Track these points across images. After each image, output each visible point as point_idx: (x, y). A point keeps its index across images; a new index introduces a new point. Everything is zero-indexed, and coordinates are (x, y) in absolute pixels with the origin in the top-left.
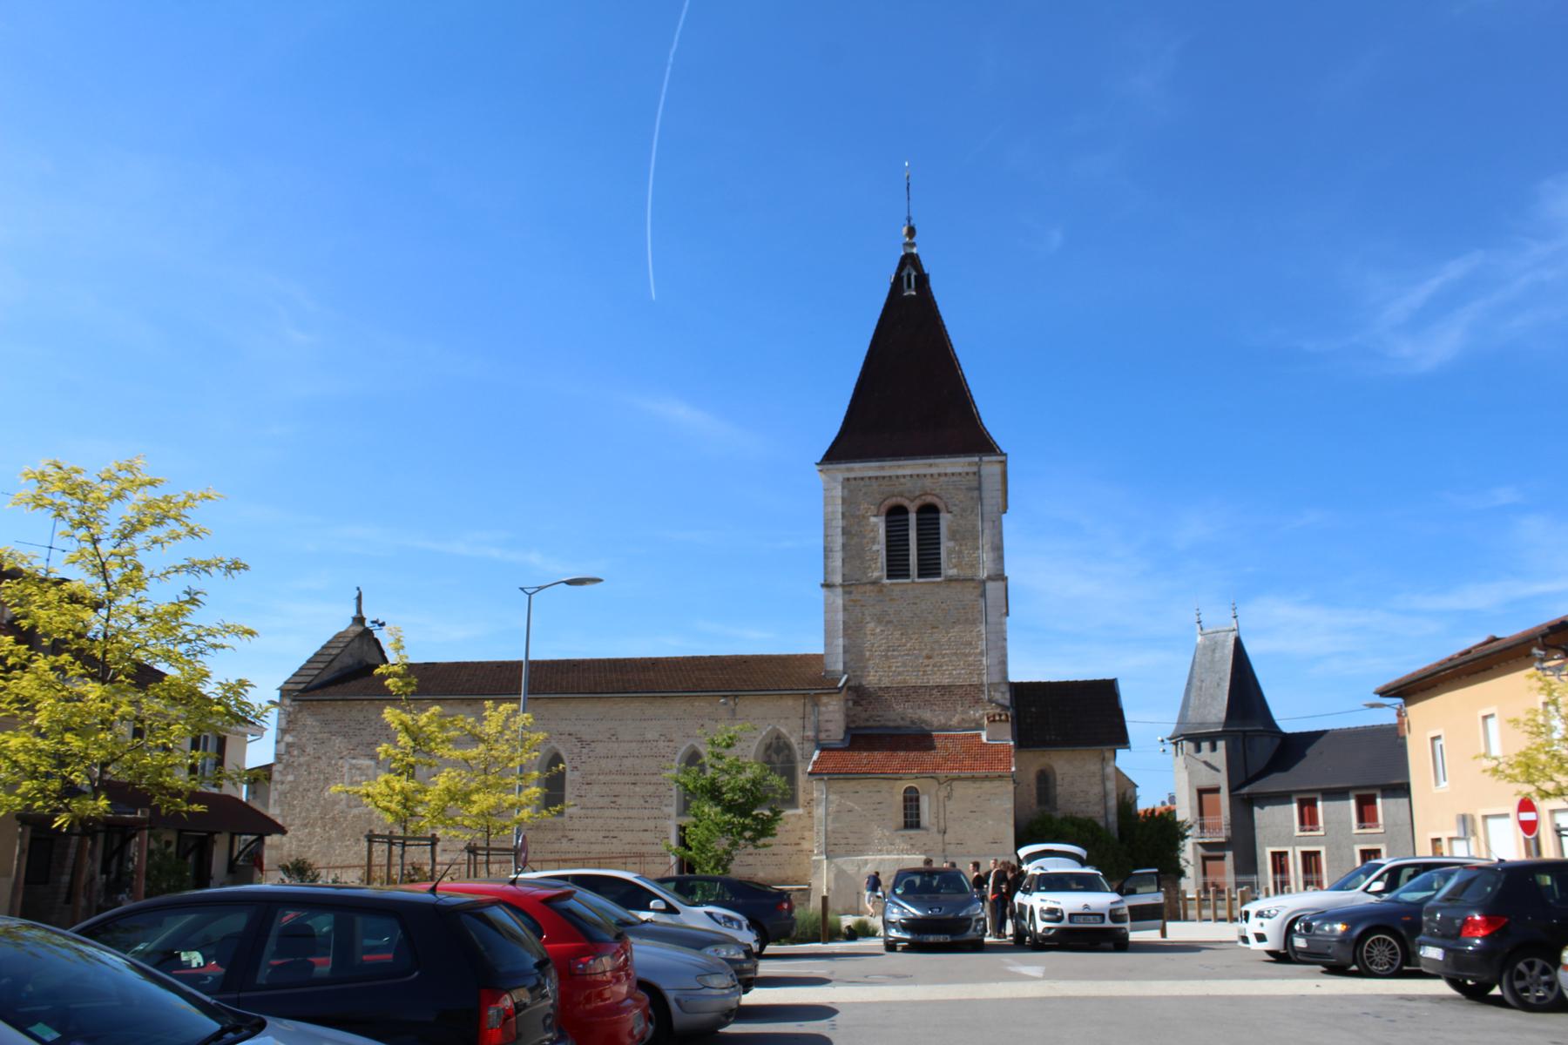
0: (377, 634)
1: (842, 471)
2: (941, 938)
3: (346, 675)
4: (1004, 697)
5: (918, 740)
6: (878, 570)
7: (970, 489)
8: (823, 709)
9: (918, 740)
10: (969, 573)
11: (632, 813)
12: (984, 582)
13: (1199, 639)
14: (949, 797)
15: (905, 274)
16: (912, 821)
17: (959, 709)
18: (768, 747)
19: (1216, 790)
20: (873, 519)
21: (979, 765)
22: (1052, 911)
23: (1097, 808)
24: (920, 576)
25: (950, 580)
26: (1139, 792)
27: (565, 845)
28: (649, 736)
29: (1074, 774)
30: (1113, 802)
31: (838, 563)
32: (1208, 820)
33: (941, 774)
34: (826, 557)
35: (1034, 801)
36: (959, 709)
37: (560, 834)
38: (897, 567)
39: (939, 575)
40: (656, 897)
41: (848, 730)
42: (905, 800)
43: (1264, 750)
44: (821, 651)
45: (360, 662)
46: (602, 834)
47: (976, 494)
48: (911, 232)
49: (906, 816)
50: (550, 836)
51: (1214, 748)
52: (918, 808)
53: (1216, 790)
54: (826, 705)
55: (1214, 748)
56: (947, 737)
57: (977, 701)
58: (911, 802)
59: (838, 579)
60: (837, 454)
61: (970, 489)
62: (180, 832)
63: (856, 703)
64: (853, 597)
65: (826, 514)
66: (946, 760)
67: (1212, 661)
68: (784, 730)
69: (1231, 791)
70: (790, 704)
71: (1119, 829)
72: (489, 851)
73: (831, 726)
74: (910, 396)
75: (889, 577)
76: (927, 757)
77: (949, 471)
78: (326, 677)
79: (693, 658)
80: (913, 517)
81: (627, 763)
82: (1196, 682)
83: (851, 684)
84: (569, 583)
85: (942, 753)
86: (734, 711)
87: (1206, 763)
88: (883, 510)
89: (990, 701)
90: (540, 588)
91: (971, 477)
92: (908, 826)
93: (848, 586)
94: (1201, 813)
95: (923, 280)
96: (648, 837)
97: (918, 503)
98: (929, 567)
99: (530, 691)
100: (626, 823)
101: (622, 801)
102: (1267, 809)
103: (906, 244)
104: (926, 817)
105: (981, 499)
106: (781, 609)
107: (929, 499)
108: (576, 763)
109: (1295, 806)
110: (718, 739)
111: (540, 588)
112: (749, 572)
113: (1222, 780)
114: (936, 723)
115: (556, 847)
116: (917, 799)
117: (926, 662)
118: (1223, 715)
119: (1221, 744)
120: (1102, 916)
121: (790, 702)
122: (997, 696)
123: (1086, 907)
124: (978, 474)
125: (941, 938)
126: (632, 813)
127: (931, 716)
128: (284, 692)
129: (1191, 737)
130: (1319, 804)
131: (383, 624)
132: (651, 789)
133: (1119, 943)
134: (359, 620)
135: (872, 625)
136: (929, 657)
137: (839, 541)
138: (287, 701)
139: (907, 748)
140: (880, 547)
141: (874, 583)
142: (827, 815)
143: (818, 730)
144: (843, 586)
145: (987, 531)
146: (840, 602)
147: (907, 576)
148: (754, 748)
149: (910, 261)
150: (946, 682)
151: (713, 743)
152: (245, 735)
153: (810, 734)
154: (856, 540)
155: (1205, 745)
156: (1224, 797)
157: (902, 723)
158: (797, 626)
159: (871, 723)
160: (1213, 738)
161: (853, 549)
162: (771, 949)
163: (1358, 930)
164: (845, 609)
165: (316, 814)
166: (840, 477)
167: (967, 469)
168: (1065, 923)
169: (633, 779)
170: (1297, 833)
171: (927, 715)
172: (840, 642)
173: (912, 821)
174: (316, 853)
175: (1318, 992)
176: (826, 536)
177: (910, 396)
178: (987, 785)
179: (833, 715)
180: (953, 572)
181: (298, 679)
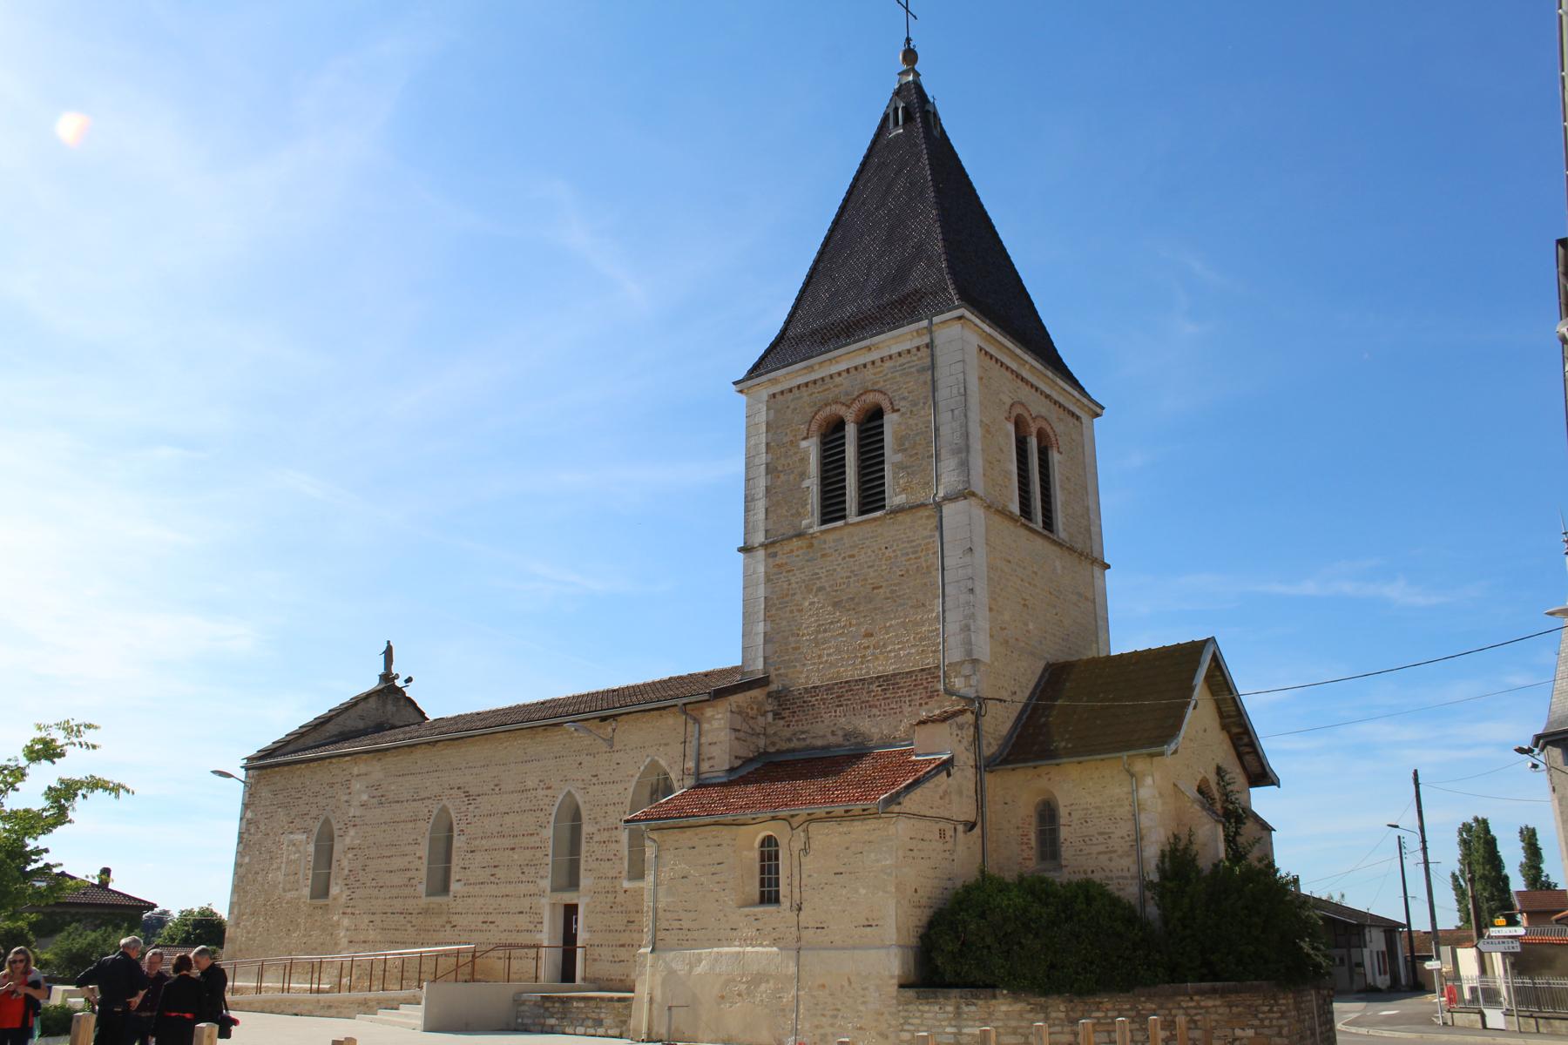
6: (811, 519)
7: (922, 370)
10: (920, 497)
11: (509, 889)
14: (805, 850)
17: (907, 709)
24: (861, 512)
25: (900, 510)
28: (530, 784)
31: (762, 516)
34: (747, 510)
36: (907, 709)
37: (445, 919)
38: (832, 509)
44: (1252, 790)
46: (481, 918)
48: (910, 56)
49: (762, 884)
54: (709, 721)
57: (932, 694)
58: (769, 853)
59: (760, 538)
61: (922, 370)
63: (777, 715)
64: (778, 560)
65: (748, 449)
73: (715, 751)
77: (894, 350)
80: (851, 431)
81: (508, 820)
88: (814, 427)
96: (522, 921)
97: (856, 406)
98: (872, 499)
100: (504, 902)
101: (500, 873)
102: (1277, 865)
107: (871, 398)
108: (463, 826)
117: (865, 642)
124: (930, 346)
126: (509, 889)
127: (872, 726)
130: (1222, 855)
131: (409, 680)
132: (528, 853)
134: (387, 677)
136: (869, 635)
137: (762, 483)
140: (812, 483)
146: (761, 569)
149: (913, 110)
150: (890, 669)
153: (691, 764)
154: (783, 477)
157: (832, 740)
159: (794, 744)
164: (768, 580)
165: (261, 901)
166: (764, 394)
169: (508, 842)
176: (747, 480)
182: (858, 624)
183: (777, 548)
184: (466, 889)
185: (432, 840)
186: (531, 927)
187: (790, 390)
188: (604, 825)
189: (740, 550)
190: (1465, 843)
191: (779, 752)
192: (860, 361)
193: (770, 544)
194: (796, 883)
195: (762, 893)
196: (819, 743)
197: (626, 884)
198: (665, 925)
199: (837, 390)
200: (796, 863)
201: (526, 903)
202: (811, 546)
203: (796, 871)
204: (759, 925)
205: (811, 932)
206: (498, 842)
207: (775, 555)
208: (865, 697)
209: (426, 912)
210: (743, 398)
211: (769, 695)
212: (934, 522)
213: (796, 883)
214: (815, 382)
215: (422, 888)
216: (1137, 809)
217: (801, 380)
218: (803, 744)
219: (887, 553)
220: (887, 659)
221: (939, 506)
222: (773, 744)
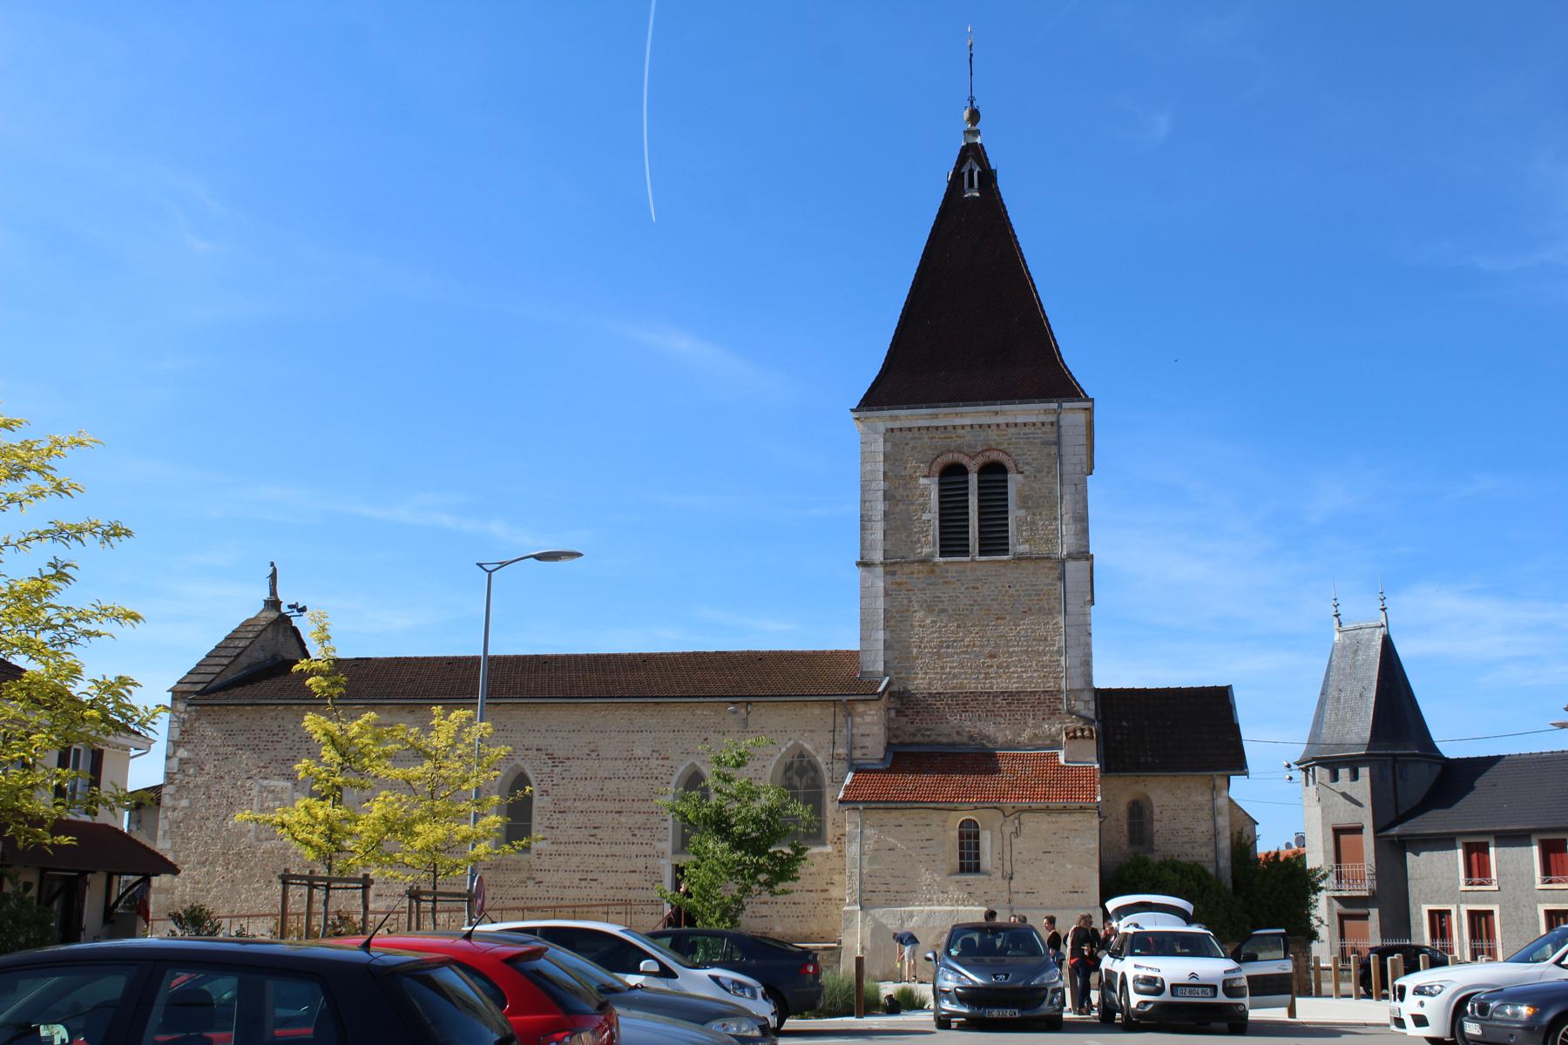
0: (296, 622)
1: (884, 419)
2: (1008, 1013)
3: (256, 674)
4: (1088, 708)
5: (977, 760)
6: (929, 545)
7: (1046, 443)
8: (858, 720)
9: (977, 760)
10: (1043, 549)
11: (617, 849)
12: (1063, 562)
13: (1337, 636)
14: (1017, 833)
15: (965, 170)
16: (969, 863)
17: (1031, 722)
18: (788, 768)
19: (1358, 830)
20: (922, 481)
21: (1055, 793)
22: (1149, 981)
23: (1204, 850)
24: (981, 553)
25: (1020, 558)
27: (531, 889)
28: (638, 752)
30: (1225, 843)
31: (879, 535)
33: (1008, 804)
34: (863, 528)
36: (1031, 722)
37: (524, 875)
38: (952, 542)
39: (1006, 552)
40: (648, 956)
41: (889, 746)
42: (961, 836)
43: (1420, 780)
44: (854, 645)
45: (274, 657)
46: (579, 875)
47: (1054, 449)
48: (975, 116)
49: (961, 856)
50: (514, 878)
51: (1355, 777)
52: (977, 846)
54: (861, 715)
55: (1355, 777)
57: (1054, 712)
58: (969, 839)
59: (878, 556)
60: (874, 400)
61: (1046, 443)
62: (43, 871)
63: (899, 713)
65: (863, 474)
66: (1013, 786)
67: (1353, 666)
68: (808, 746)
69: (1376, 831)
70: (816, 714)
72: (435, 896)
73: (868, 742)
74: (971, 323)
75: (942, 554)
76: (989, 781)
77: (1020, 420)
78: (230, 675)
80: (973, 479)
81: (611, 786)
82: (1332, 692)
83: (894, 688)
84: (539, 557)
86: (745, 721)
87: (1344, 795)
88: (936, 468)
89: (1070, 712)
90: (503, 564)
91: (1048, 428)
93: (890, 565)
95: (988, 178)
97: (980, 460)
98: (994, 542)
100: (609, 862)
102: (1424, 855)
103: (967, 132)
104: (987, 860)
107: (994, 456)
108: (547, 786)
109: (1460, 852)
111: (503, 564)
113: (1365, 817)
114: (1000, 740)
115: (521, 891)
116: (977, 836)
118: (1367, 735)
119: (1364, 772)
120: (1214, 987)
121: (817, 711)
122: (1079, 706)
123: (1193, 976)
124: (1056, 424)
125: (1008, 1013)
126: (617, 849)
127: (996, 731)
128: (177, 694)
129: (1325, 762)
130: (1492, 850)
131: (303, 609)
132: (640, 819)
133: (1237, 1024)
134: (273, 603)
135: (920, 614)
136: (992, 656)
137: (880, 507)
138: (181, 706)
140: (932, 516)
141: (923, 561)
144: (884, 564)
145: (1067, 498)
146: (880, 584)
147: (966, 553)
148: (770, 769)
149: (972, 153)
150: (1013, 687)
151: (719, 761)
152: (127, 749)
153: (842, 751)
154: (901, 506)
155: (1344, 773)
156: (1368, 837)
157: (957, 738)
160: (1353, 764)
162: (791, 1023)
164: (886, 594)
166: (882, 427)
167: (1043, 418)
168: (1166, 997)
169: (610, 806)
170: (1463, 887)
171: (989, 729)
172: (881, 635)
173: (969, 863)
174: (215, 898)
176: (863, 501)
180: (1023, 548)
181: (196, 678)
182: (982, 646)
183: (897, 568)
184: (555, 847)
186: (648, 885)
187: (910, 429)
189: (858, 564)
191: (901, 744)
192: (986, 420)
193: (892, 563)
194: (1007, 857)
195: (962, 865)
196: (944, 740)
198: (870, 887)
199: (959, 441)
200: (1007, 843)
201: (640, 863)
202: (933, 571)
203: (1007, 850)
204: (971, 889)
205: (1021, 896)
206: (599, 805)
207: (894, 573)
208: (990, 706)
212: (1055, 574)
213: (1007, 857)
214: (937, 428)
218: (927, 739)
219: (1011, 591)
220: (1010, 678)
221: (1063, 562)
222: (896, 736)
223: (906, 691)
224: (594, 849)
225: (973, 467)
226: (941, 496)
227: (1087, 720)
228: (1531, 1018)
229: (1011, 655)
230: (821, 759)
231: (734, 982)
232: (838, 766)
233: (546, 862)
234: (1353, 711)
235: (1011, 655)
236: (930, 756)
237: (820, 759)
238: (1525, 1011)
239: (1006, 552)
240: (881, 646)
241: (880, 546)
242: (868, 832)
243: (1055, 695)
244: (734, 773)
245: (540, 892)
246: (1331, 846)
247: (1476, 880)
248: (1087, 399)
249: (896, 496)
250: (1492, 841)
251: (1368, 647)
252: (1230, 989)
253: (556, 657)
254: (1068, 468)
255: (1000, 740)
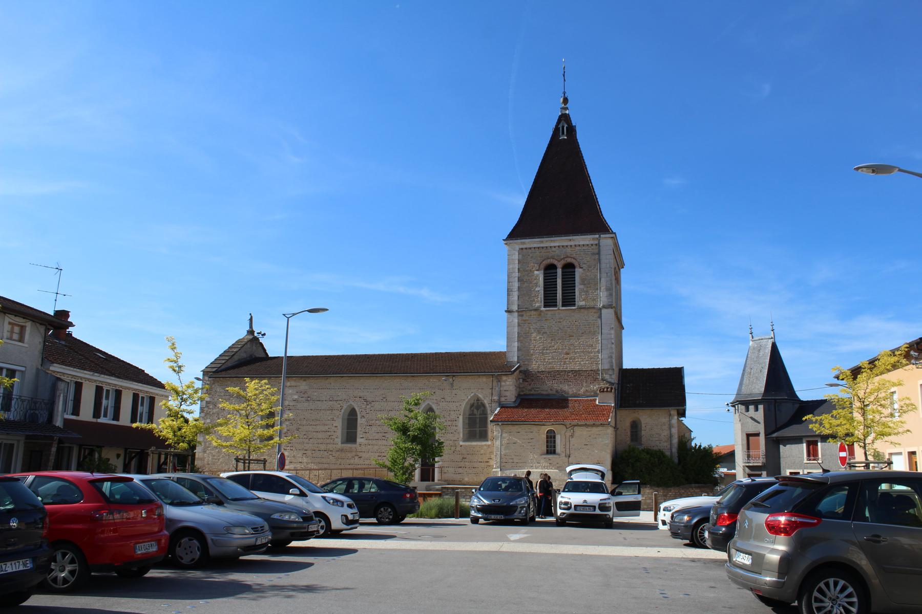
0: (261, 340)
1: (518, 244)
2: (499, 517)
3: (245, 361)
4: (614, 378)
5: (559, 402)
6: (539, 302)
7: (593, 254)
8: (503, 383)
9: (559, 402)
10: (592, 304)
12: (600, 309)
13: (751, 343)
14: (572, 436)
15: (560, 126)
16: (551, 450)
17: (585, 384)
18: (472, 406)
19: (758, 435)
20: (536, 272)
21: (594, 415)
22: (566, 503)
23: (665, 444)
24: (563, 306)
25: (581, 308)
26: (693, 435)
27: (357, 460)
29: (655, 426)
30: (675, 441)
31: (516, 298)
32: (752, 452)
33: (567, 422)
34: (508, 295)
35: (628, 439)
36: (585, 384)
37: (354, 454)
38: (549, 301)
39: (574, 305)
40: (295, 487)
41: (519, 396)
42: (547, 437)
43: (788, 410)
44: (504, 350)
45: (251, 356)
47: (597, 257)
48: (566, 101)
50: (350, 455)
51: (757, 409)
52: (555, 442)
53: (758, 435)
54: (505, 381)
55: (757, 409)
56: (576, 401)
57: (596, 380)
58: (551, 438)
59: (515, 308)
60: (516, 233)
61: (593, 254)
62: (126, 450)
63: (524, 380)
65: (509, 269)
66: (572, 414)
67: (758, 357)
68: (480, 396)
69: (766, 435)
70: (484, 381)
71: (679, 457)
72: (250, 460)
73: (508, 394)
74: (561, 199)
75: (545, 306)
76: (560, 412)
77: (582, 243)
78: (229, 364)
79: (436, 354)
80: (559, 271)
82: (748, 370)
83: (522, 369)
84: (311, 311)
85: (570, 410)
86: (452, 384)
87: (751, 418)
88: (542, 266)
89: (603, 380)
90: (294, 314)
91: (594, 247)
92: (548, 452)
93: (520, 312)
94: (748, 448)
95: (572, 130)
97: (563, 262)
98: (569, 300)
99: (287, 373)
102: (788, 446)
103: (562, 108)
104: (559, 448)
105: (599, 260)
106: (480, 323)
107: (569, 260)
108: (364, 414)
109: (805, 445)
110: (411, 400)
111: (294, 314)
112: (467, 307)
113: (761, 428)
114: (571, 393)
115: (352, 461)
116: (554, 437)
118: (763, 389)
119: (761, 407)
120: (594, 507)
121: (484, 379)
122: (607, 377)
123: (585, 501)
124: (598, 245)
125: (499, 517)
127: (568, 388)
128: (205, 373)
129: (744, 403)
130: (819, 444)
131: (264, 334)
133: (608, 524)
134: (251, 332)
135: (534, 335)
137: (516, 285)
138: (207, 378)
139: (551, 407)
140: (540, 289)
141: (536, 310)
142: (501, 445)
143: (500, 396)
144: (518, 311)
145: (603, 280)
146: (516, 321)
147: (556, 306)
148: (463, 406)
149: (564, 118)
150: (577, 368)
151: (408, 403)
152: (167, 397)
153: (496, 398)
154: (526, 284)
155: (752, 407)
156: (762, 439)
157: (551, 392)
158: (491, 336)
160: (756, 403)
161: (524, 289)
162: (362, 520)
163: (695, 520)
164: (519, 325)
166: (517, 247)
167: (592, 242)
168: (572, 511)
170: (805, 461)
171: (566, 388)
172: (516, 344)
173: (551, 450)
174: (222, 463)
175: (659, 555)
176: (509, 282)
177: (561, 199)
178: (595, 429)
179: (509, 387)
180: (582, 303)
181: (213, 366)
185: (343, 419)
188: (448, 418)
190: (4, 398)
191: (525, 395)
192: (565, 244)
193: (521, 311)
196: (544, 393)
197: (461, 443)
209: (342, 450)
210: (506, 247)
211: (520, 372)
212: (597, 315)
215: (339, 440)
216: (670, 427)
217: (535, 245)
221: (600, 309)
223: (528, 370)
224: (384, 442)
225: (559, 266)
226: (545, 279)
227: (613, 384)
228: (688, 522)
229: (576, 353)
230: (486, 402)
231: (333, 499)
232: (493, 405)
233: (364, 448)
234: (757, 378)
235: (576, 353)
236: (537, 400)
237: (486, 401)
238: (686, 518)
239: (574, 305)
240: (516, 349)
241: (516, 303)
242: (504, 435)
243: (596, 372)
244: (413, 408)
245: (361, 462)
246: (745, 442)
247: (812, 458)
248: (613, 233)
249: (524, 279)
250: (819, 440)
251: (765, 348)
252: (603, 507)
253: (374, 355)
254: (603, 266)
255: (571, 393)
